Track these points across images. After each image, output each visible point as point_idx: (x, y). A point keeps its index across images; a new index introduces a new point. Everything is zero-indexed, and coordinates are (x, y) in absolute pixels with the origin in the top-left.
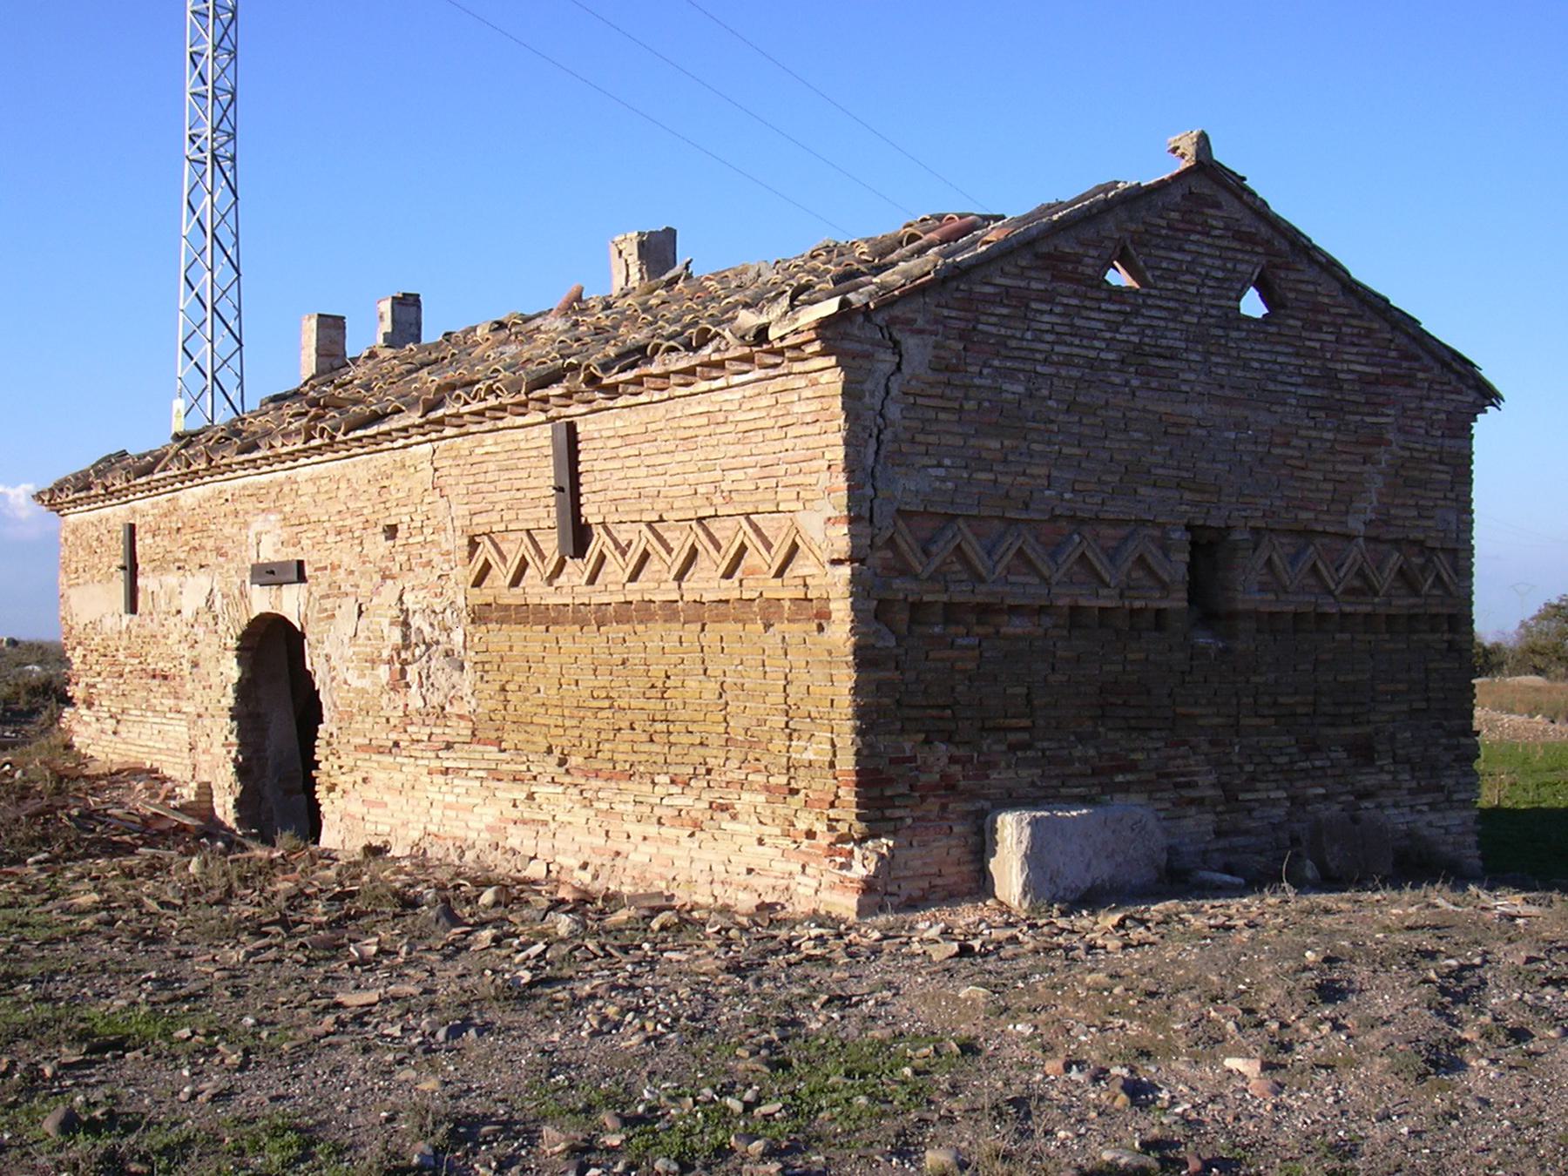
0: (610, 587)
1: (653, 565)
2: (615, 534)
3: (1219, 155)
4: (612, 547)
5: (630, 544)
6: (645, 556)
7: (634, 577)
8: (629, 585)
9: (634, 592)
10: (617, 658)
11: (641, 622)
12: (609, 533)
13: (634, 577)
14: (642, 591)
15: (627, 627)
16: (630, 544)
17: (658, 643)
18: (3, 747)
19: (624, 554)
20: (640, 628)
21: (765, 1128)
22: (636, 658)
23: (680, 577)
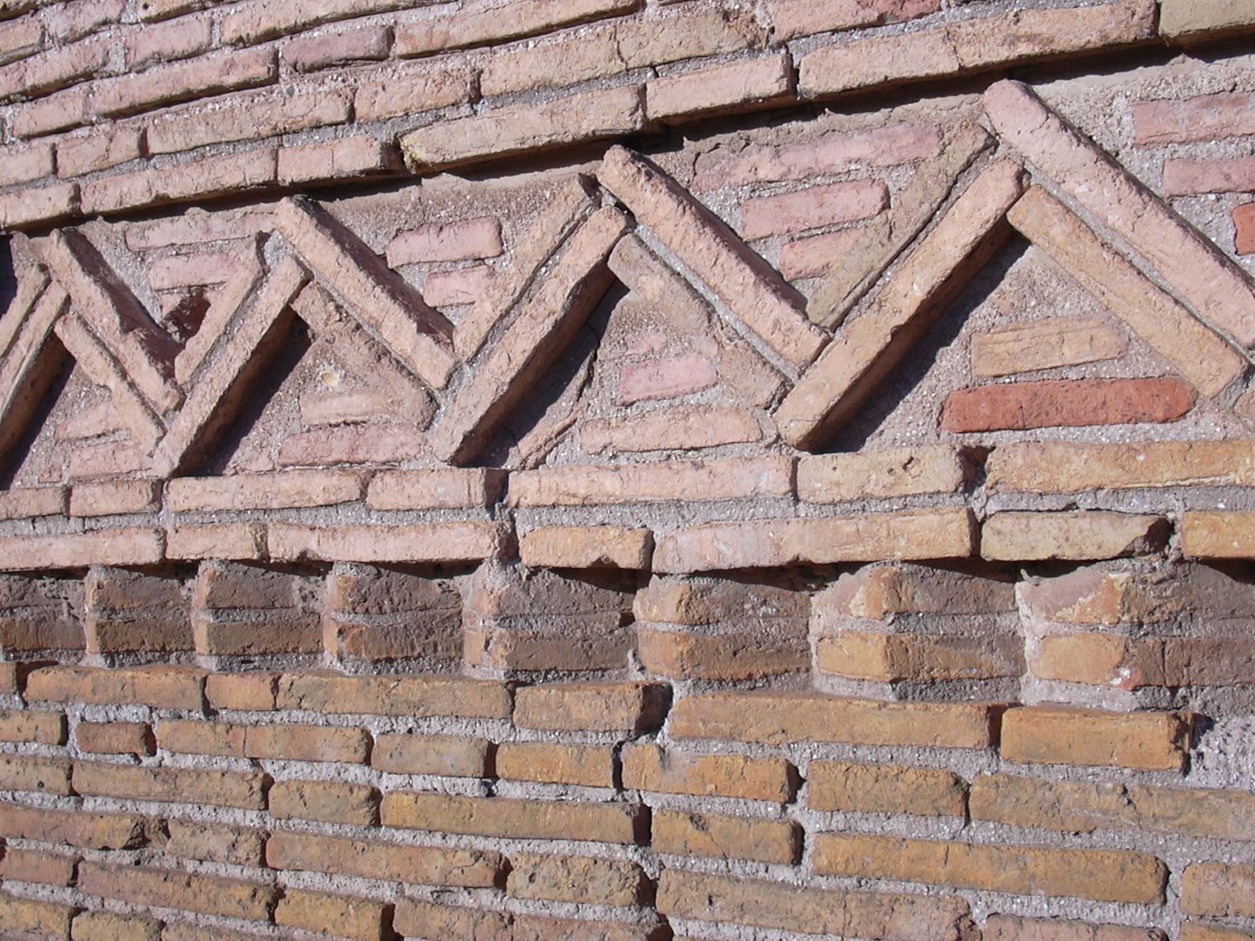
0: (87, 499)
1: (323, 394)
2: (122, 269)
3: (991, 458)
4: (106, 317)
5: (192, 311)
6: (287, 343)
7: (207, 456)
8: (186, 492)
9: (214, 522)
10: (107, 813)
11: (238, 660)
12: (90, 260)
13: (207, 456)
14: (259, 517)
15: (162, 680)
16: (192, 311)
17: (336, 766)
18: (5, 715)
19: (163, 351)
20: (241, 691)
21: (613, 402)
22: (212, 829)
23: (488, 446)
